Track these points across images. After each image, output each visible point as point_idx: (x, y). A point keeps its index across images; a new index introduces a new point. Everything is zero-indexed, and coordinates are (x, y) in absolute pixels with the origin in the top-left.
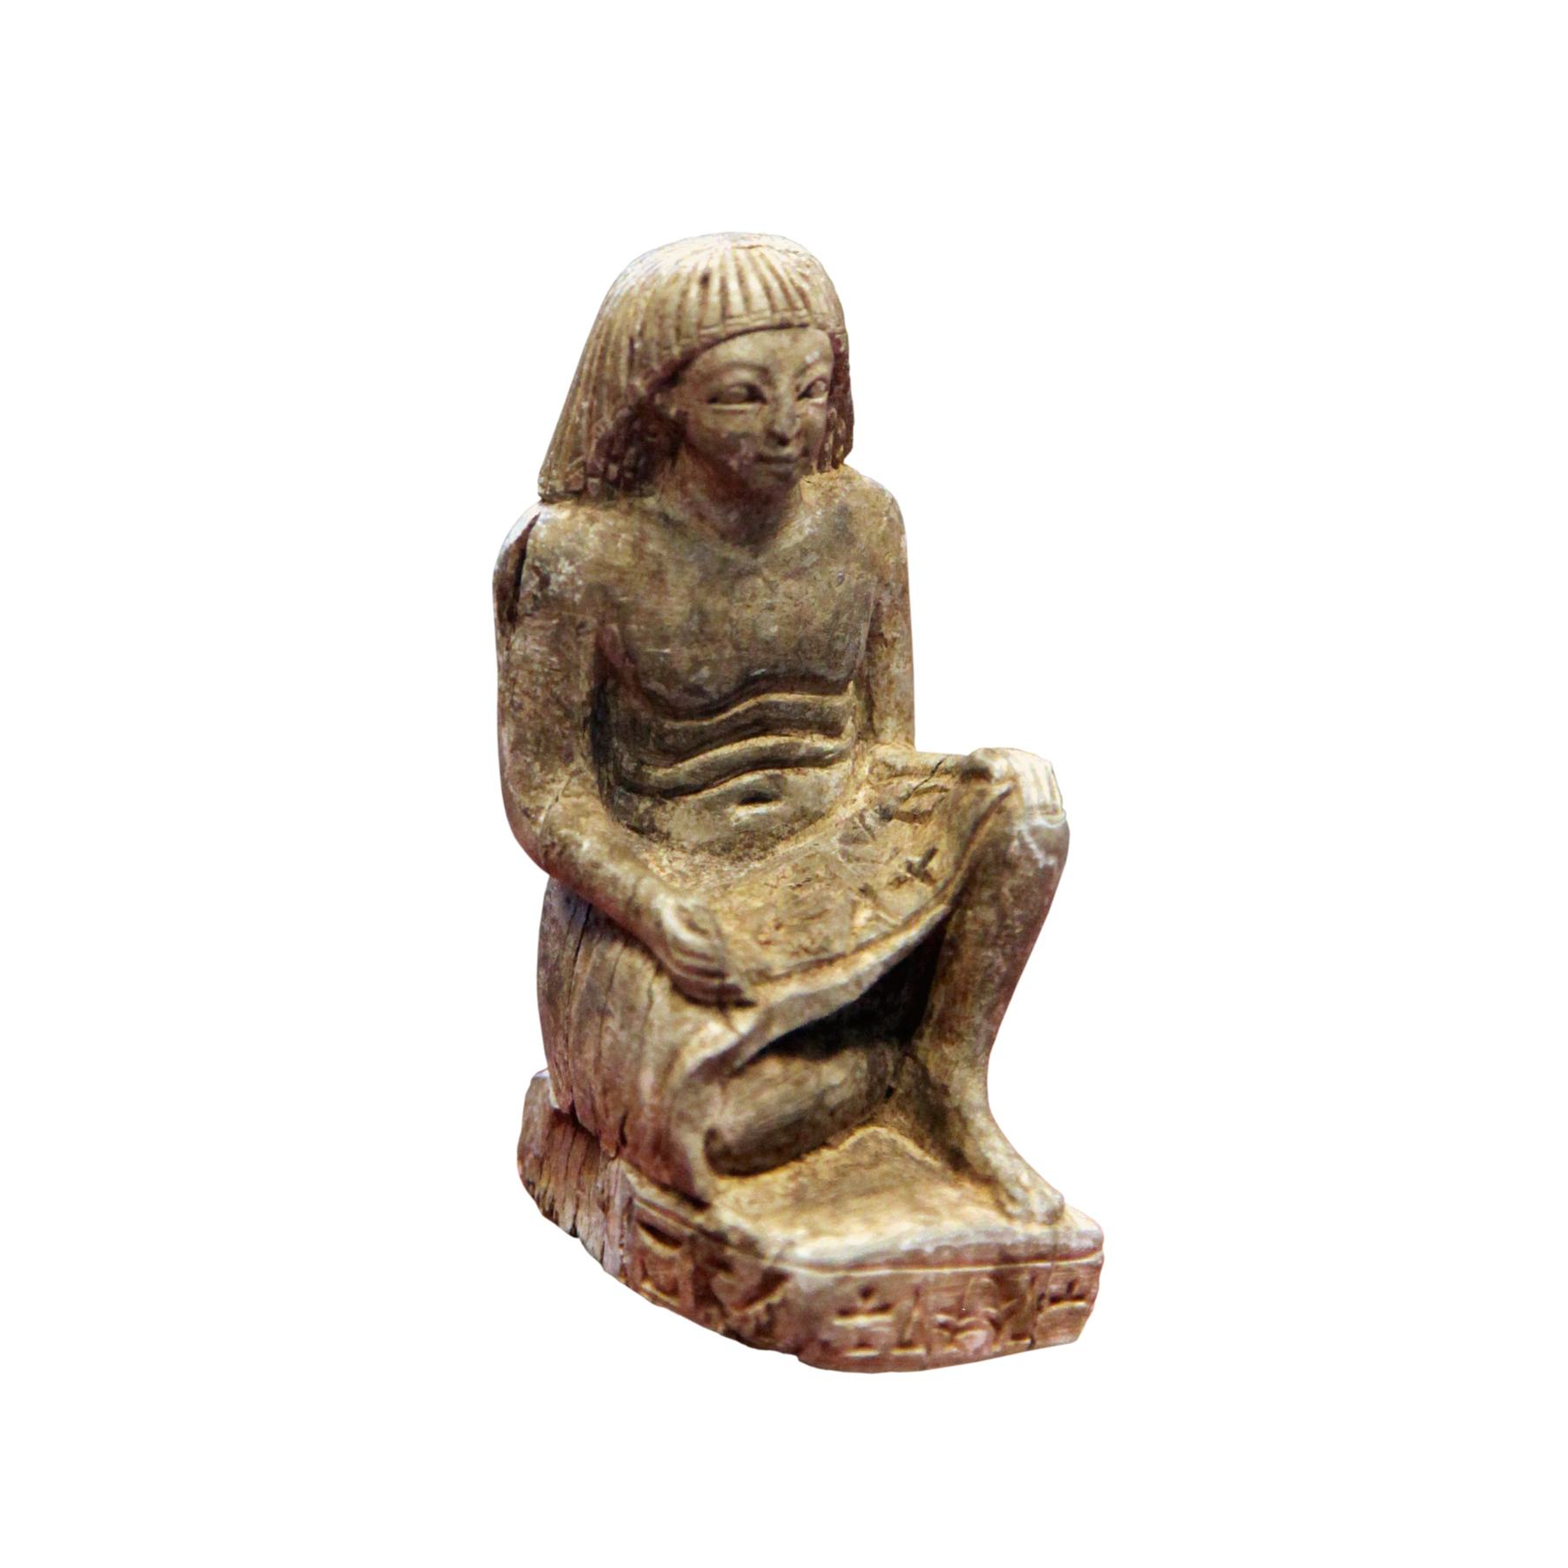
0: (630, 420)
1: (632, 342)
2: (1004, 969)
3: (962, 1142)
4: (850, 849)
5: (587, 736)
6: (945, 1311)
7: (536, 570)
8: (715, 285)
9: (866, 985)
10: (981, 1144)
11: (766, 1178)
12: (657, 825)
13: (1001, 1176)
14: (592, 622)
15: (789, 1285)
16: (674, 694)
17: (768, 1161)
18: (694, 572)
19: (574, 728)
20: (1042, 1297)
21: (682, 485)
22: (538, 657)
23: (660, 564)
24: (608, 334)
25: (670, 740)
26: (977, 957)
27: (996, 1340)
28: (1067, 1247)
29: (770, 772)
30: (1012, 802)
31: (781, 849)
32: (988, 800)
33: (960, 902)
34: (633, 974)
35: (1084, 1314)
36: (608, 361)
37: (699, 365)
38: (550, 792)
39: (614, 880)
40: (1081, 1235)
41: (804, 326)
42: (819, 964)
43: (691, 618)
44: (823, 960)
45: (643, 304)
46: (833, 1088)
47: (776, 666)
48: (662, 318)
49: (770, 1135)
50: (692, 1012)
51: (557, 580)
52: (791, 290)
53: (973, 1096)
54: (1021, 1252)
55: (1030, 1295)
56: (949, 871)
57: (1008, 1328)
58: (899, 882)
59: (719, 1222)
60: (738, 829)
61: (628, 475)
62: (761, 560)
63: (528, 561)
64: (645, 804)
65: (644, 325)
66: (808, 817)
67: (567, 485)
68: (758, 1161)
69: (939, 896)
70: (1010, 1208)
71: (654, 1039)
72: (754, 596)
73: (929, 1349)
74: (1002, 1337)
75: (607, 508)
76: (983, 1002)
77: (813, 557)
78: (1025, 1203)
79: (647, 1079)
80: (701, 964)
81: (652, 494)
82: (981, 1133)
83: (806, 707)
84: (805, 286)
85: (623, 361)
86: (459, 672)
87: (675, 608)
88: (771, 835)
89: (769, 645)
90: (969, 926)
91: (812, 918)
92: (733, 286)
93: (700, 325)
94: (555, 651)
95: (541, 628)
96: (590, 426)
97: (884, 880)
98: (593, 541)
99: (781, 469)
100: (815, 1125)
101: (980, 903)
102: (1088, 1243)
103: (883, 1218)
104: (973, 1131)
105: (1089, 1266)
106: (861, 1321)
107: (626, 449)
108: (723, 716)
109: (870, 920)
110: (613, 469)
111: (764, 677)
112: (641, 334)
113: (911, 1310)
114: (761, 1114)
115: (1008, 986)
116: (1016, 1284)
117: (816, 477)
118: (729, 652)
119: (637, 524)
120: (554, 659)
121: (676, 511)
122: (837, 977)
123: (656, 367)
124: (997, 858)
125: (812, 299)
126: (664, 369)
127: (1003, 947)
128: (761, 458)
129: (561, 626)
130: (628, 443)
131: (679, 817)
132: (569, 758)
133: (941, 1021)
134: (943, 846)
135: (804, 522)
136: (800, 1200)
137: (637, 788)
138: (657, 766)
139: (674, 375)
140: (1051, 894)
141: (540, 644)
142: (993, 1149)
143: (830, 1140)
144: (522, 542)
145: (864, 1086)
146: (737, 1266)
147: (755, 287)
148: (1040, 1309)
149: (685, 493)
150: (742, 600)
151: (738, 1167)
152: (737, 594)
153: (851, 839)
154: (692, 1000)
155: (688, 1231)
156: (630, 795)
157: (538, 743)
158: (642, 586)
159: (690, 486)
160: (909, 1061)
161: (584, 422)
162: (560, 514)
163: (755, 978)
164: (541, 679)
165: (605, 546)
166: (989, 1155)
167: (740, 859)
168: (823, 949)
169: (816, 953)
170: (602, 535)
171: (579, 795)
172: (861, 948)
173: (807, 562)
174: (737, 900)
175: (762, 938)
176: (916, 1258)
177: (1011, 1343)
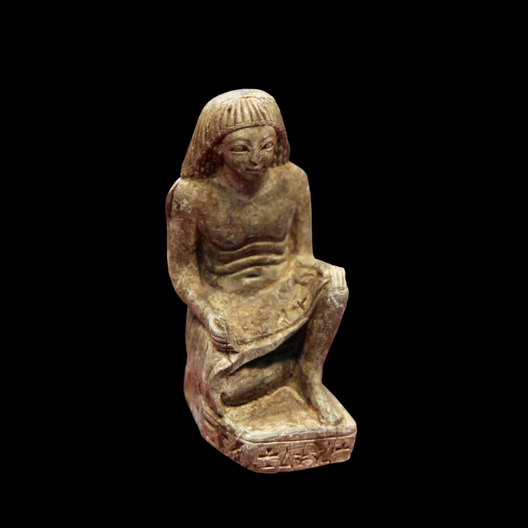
0: (206, 155)
1: (206, 130)
2: (326, 339)
3: (310, 395)
4: (281, 294)
5: (194, 255)
6: (297, 454)
7: (176, 202)
8: (233, 112)
9: (278, 345)
10: (316, 397)
11: (243, 407)
12: (218, 284)
13: (321, 409)
14: (194, 220)
15: (243, 446)
16: (222, 244)
17: (245, 401)
18: (228, 205)
19: (190, 253)
20: (333, 448)
21: (225, 175)
22: (177, 230)
23: (217, 202)
25: (222, 258)
27: (316, 463)
28: (341, 432)
29: (257, 267)
30: (329, 286)
31: (261, 292)
32: (321, 285)
33: (312, 317)
34: (204, 338)
36: (199, 135)
37: (227, 138)
38: (181, 274)
39: (198, 307)
40: (347, 429)
41: (263, 125)
42: (263, 337)
43: (227, 220)
44: (264, 336)
45: (210, 117)
46: (268, 377)
47: (257, 234)
48: (215, 122)
49: (244, 394)
50: (218, 354)
51: (183, 206)
52: (259, 112)
54: (325, 435)
56: (308, 307)
57: (321, 458)
58: (294, 308)
59: (225, 422)
60: (246, 286)
61: (208, 171)
62: (252, 199)
63: (174, 199)
64: (215, 277)
65: (210, 124)
66: (269, 282)
67: (188, 173)
68: (241, 402)
69: (305, 314)
70: (322, 421)
71: (206, 362)
72: (249, 212)
73: (292, 466)
74: (319, 461)
75: (200, 182)
76: (320, 349)
77: (271, 198)
78: (327, 419)
79: (204, 375)
80: (220, 339)
81: (215, 177)
82: (317, 393)
83: (269, 246)
84: (265, 111)
85: (203, 135)
87: (222, 216)
88: (256, 287)
89: (255, 228)
90: (315, 325)
91: (264, 320)
92: (239, 112)
93: (227, 126)
94: (182, 228)
95: (178, 221)
96: (194, 155)
97: (290, 307)
98: (195, 193)
99: (255, 173)
100: (261, 389)
101: (318, 318)
103: (278, 424)
104: (314, 392)
106: (268, 458)
107: (206, 163)
108: (240, 250)
109: (282, 321)
110: (203, 169)
111: (252, 238)
112: (209, 127)
113: (285, 454)
114: (240, 387)
116: (323, 445)
117: (276, 169)
118: (240, 230)
119: (210, 188)
120: (182, 231)
121: (223, 183)
122: (269, 342)
123: (213, 138)
124: (323, 304)
125: (267, 116)
126: (216, 139)
127: (326, 332)
128: (247, 169)
129: (184, 221)
130: (207, 161)
131: (226, 282)
132: (187, 263)
133: (307, 354)
134: (308, 298)
136: (253, 416)
137: (212, 271)
138: (219, 265)
139: (219, 141)
141: (177, 226)
142: (320, 399)
143: (268, 393)
145: (280, 375)
146: (229, 438)
147: (246, 111)
148: (332, 452)
149: (226, 177)
150: (245, 213)
151: (234, 404)
152: (243, 211)
153: (283, 291)
154: (219, 350)
155: (216, 424)
157: (177, 258)
158: (210, 209)
159: (228, 175)
160: (297, 366)
161: (192, 154)
163: (239, 343)
164: (178, 237)
165: (199, 195)
166: (318, 401)
167: (246, 296)
168: (265, 332)
169: (262, 333)
170: (198, 191)
171: (191, 275)
172: (278, 332)
173: (269, 199)
174: (241, 312)
175: (245, 328)
176: (286, 438)
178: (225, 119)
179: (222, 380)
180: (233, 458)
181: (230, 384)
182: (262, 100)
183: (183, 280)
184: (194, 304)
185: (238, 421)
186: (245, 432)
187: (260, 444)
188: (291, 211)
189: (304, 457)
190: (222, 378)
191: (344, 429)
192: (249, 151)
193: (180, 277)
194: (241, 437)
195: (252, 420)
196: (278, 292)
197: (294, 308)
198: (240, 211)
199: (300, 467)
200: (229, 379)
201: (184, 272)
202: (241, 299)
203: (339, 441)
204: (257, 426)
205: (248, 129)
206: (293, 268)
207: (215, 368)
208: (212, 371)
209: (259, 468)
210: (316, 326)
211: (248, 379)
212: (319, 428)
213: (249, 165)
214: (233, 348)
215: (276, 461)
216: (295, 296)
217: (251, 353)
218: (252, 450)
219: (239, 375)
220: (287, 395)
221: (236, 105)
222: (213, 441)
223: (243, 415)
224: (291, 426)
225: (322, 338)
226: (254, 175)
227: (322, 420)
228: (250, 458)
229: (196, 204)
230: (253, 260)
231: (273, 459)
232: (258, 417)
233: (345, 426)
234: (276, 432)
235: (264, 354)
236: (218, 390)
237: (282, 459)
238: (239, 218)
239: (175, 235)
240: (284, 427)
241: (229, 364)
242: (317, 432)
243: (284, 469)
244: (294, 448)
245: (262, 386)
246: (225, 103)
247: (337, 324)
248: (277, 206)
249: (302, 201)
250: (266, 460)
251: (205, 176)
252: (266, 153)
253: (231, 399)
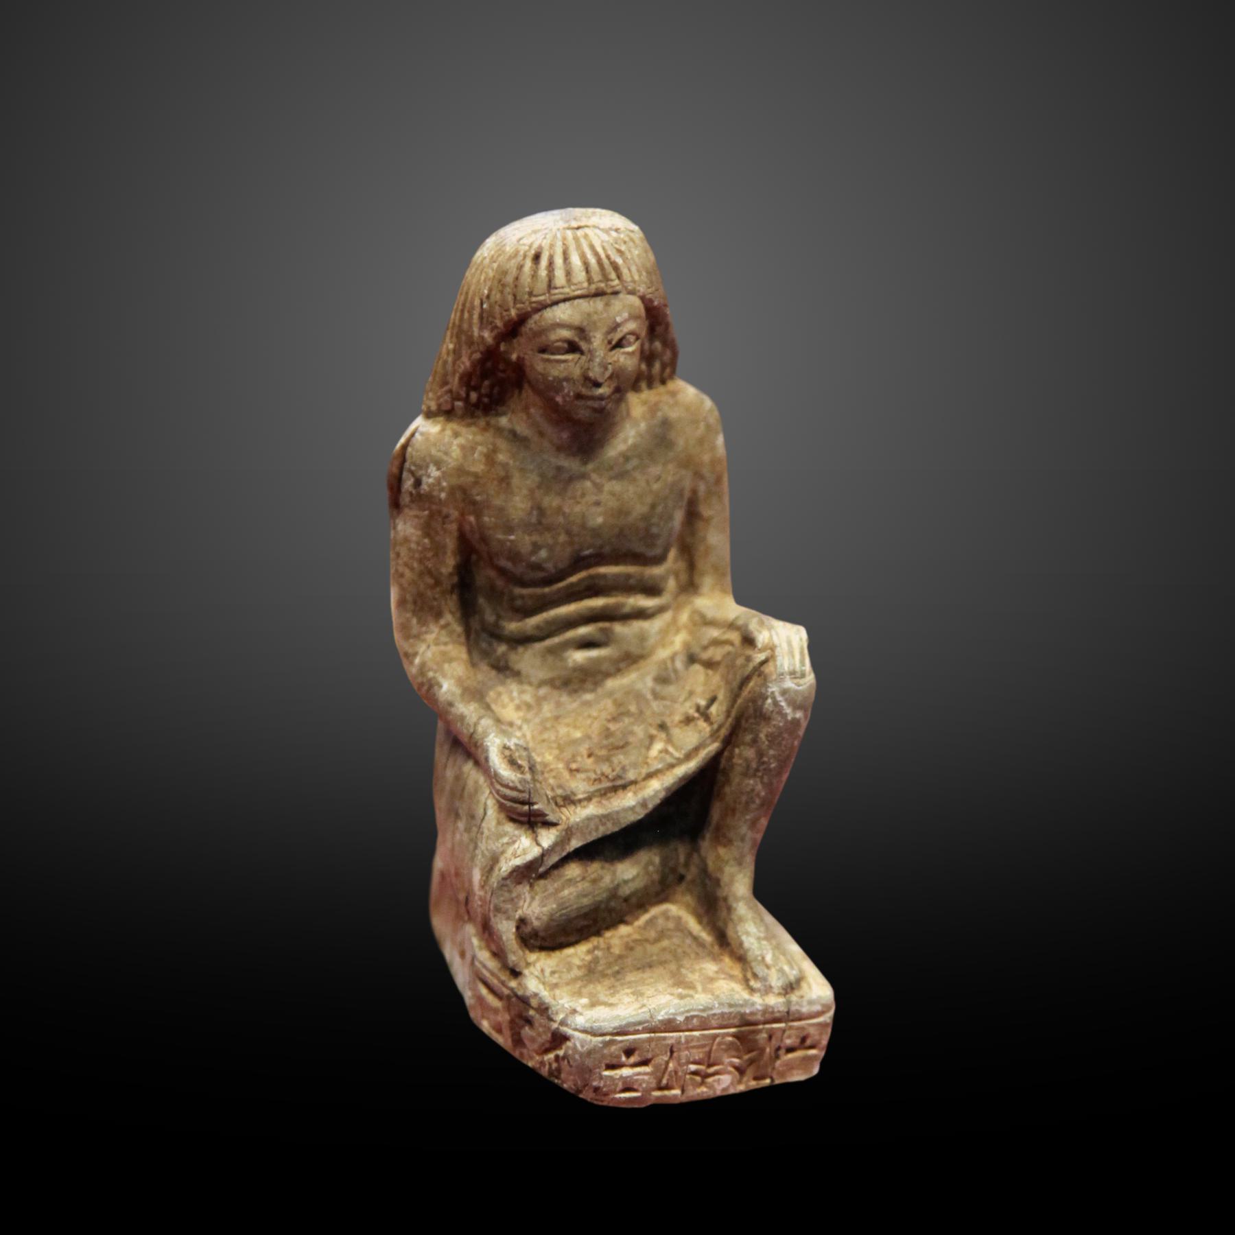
0: (482, 362)
1: (482, 304)
2: (763, 794)
3: (726, 924)
4: (658, 688)
5: (455, 597)
6: (695, 1063)
7: (412, 473)
8: (544, 262)
9: (651, 806)
10: (739, 928)
11: (569, 951)
12: (510, 664)
13: (750, 956)
14: (455, 514)
15: (569, 1044)
16: (519, 570)
17: (572, 939)
18: (533, 479)
19: (443, 593)
20: (779, 1049)
21: (526, 409)
22: (414, 538)
23: (507, 472)
25: (519, 603)
27: (740, 1082)
28: (798, 1011)
29: (601, 625)
30: (769, 669)
31: (610, 684)
32: (751, 666)
33: (730, 741)
34: (477, 790)
36: (466, 315)
37: (531, 324)
38: (424, 641)
39: (462, 718)
40: (811, 1002)
41: (616, 293)
42: (615, 789)
43: (530, 514)
44: (618, 786)
45: (491, 274)
46: (626, 882)
47: (601, 547)
48: (504, 286)
49: (570, 921)
50: (509, 828)
51: (427, 482)
52: (605, 261)
54: (759, 1017)
56: (721, 718)
57: (750, 1072)
58: (688, 720)
59: (526, 988)
60: (575, 669)
61: (486, 400)
62: (590, 466)
63: (407, 465)
64: (502, 649)
65: (490, 290)
66: (630, 659)
67: (439, 406)
68: (563, 939)
69: (714, 735)
70: (754, 984)
71: (482, 846)
72: (583, 495)
73: (683, 1091)
74: (745, 1079)
75: (469, 425)
76: (748, 817)
77: (635, 462)
78: (764, 979)
79: (477, 876)
80: (514, 794)
81: (504, 414)
82: (741, 919)
83: (629, 576)
84: (619, 261)
85: (476, 317)
87: (518, 505)
88: (600, 672)
89: (596, 532)
90: (736, 760)
91: (617, 748)
92: (559, 261)
93: (531, 294)
94: (427, 534)
95: (417, 517)
96: (454, 363)
97: (677, 718)
98: (456, 452)
99: (596, 404)
100: (610, 911)
101: (744, 744)
103: (649, 991)
104: (734, 917)
106: (626, 1072)
107: (483, 381)
108: (561, 585)
109: (661, 752)
110: (474, 396)
111: (590, 556)
112: (488, 297)
113: (667, 1063)
114: (562, 906)
116: (756, 1041)
117: (646, 394)
118: (562, 538)
119: (491, 439)
120: (426, 541)
121: (522, 429)
122: (628, 800)
123: (499, 323)
124: (755, 711)
125: (625, 271)
126: (505, 325)
127: (762, 778)
128: (579, 396)
129: (431, 516)
130: (484, 376)
131: (528, 660)
132: (438, 615)
133: (718, 828)
134: (721, 696)
136: (591, 972)
137: (496, 635)
138: (511, 620)
139: (513, 329)
141: (415, 528)
142: (748, 933)
143: (628, 918)
145: (656, 877)
146: (536, 1024)
147: (576, 260)
148: (777, 1057)
149: (528, 414)
150: (574, 498)
151: (546, 944)
152: (569, 494)
153: (663, 680)
154: (512, 820)
155: (506, 992)
157: (415, 603)
158: (492, 488)
159: (532, 410)
160: (695, 856)
161: (450, 359)
163: (560, 801)
164: (417, 555)
165: (465, 457)
166: (744, 938)
167: (576, 691)
168: (619, 777)
169: (614, 780)
170: (462, 447)
171: (446, 644)
172: (650, 776)
173: (629, 466)
174: (563, 730)
175: (574, 766)
176: (670, 1025)
178: (526, 278)
179: (520, 888)
180: (544, 1072)
181: (537, 898)
182: (614, 234)
183: (429, 654)
184: (453, 710)
185: (556, 986)
186: (574, 1011)
187: (608, 1038)
188: (681, 494)
189: (712, 1070)
190: (520, 883)
191: (805, 1003)
192: (582, 353)
193: (422, 648)
194: (563, 1023)
195: (590, 982)
196: (649, 682)
197: (688, 720)
198: (562, 493)
199: (702, 1092)
200: (536, 888)
201: (430, 637)
202: (565, 698)
203: (793, 1032)
204: (602, 997)
205: (581, 301)
206: (685, 627)
207: (502, 860)
208: (496, 869)
209: (606, 1094)
210: (740, 762)
211: (580, 886)
212: (746, 1001)
213: (583, 385)
214: (545, 815)
215: (646, 1078)
216: (691, 693)
217: (588, 826)
218: (589, 1053)
219: (560, 876)
220: (671, 925)
221: (552, 246)
222: (499, 1031)
223: (569, 970)
224: (681, 997)
225: (753, 790)
226: (595, 410)
227: (752, 983)
228: (585, 1071)
229: (459, 476)
230: (592, 609)
231: (639, 1074)
232: (604, 975)
233: (807, 997)
234: (644, 1009)
235: (616, 829)
236: (511, 913)
237: (659, 1074)
238: (559, 510)
239: (410, 549)
240: (663, 999)
241: (535, 852)
242: (742, 1010)
243: (665, 1096)
244: (687, 1048)
245: (613, 904)
246: (526, 241)
247: (788, 757)
248: (648, 482)
249: (705, 471)
250: (621, 1077)
251: (479, 413)
252: (622, 359)
253: (541, 934)
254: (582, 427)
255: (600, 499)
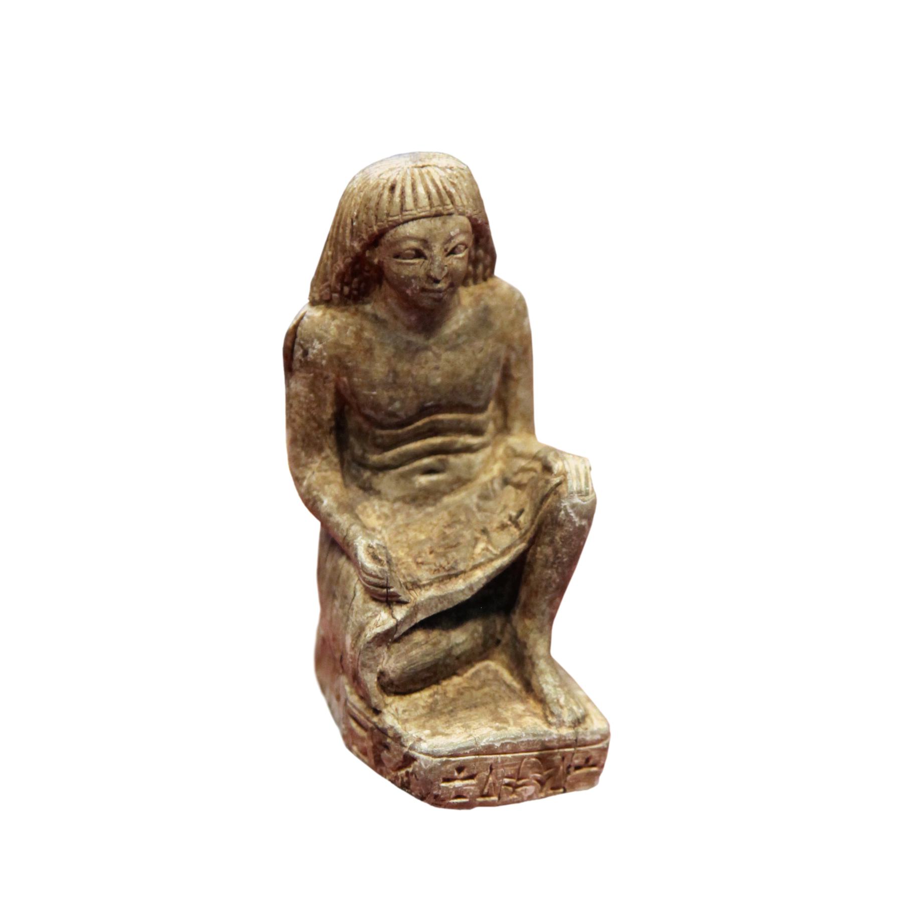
0: (353, 264)
1: (352, 222)
2: (558, 580)
3: (531, 676)
4: (481, 503)
5: (332, 436)
6: (508, 777)
7: (301, 346)
8: (398, 192)
9: (476, 589)
10: (540, 679)
11: (416, 695)
12: (373, 486)
13: (548, 699)
14: (332, 376)
15: (416, 763)
16: (379, 417)
18: (390, 350)
19: (324, 433)
20: (569, 767)
21: (385, 299)
22: (303, 394)
23: (371, 345)
24: (341, 214)
25: (379, 441)
26: (541, 573)
27: (541, 791)
28: (584, 739)
29: (439, 457)
30: (562, 489)
31: (446, 500)
32: (549, 487)
33: (533, 542)
34: (349, 577)
35: (598, 774)
36: (341, 231)
37: (388, 237)
38: (310, 468)
40: (593, 733)
41: (450, 214)
42: (449, 577)
43: (388, 376)
44: (452, 575)
45: (359, 200)
46: (458, 645)
47: (440, 400)
48: (368, 209)
49: (417, 673)
50: (372, 605)
51: (312, 353)
52: (443, 191)
53: (541, 650)
54: (555, 744)
55: (565, 765)
56: (527, 525)
57: (548, 784)
58: (503, 527)
59: (384, 722)
60: (420, 489)
61: (355, 292)
62: (432, 341)
63: (298, 340)
64: (367, 474)
65: (358, 212)
66: (461, 482)
67: (321, 297)
68: (411, 687)
69: (522, 537)
70: (551, 719)
71: (353, 618)
72: (426, 362)
73: (499, 798)
74: (545, 789)
75: (343, 311)
76: (547, 598)
77: (464, 338)
78: (559, 716)
79: (349, 641)
80: (376, 580)
81: (368, 303)
82: (542, 672)
83: (460, 421)
84: (453, 191)
85: (348, 231)
86: (264, 401)
87: (379, 369)
88: (438, 491)
89: (436, 389)
90: (538, 556)
91: (451, 547)
92: (409, 191)
93: (388, 215)
94: (312, 391)
95: (305, 378)
96: (332, 265)
97: (495, 525)
98: (333, 330)
99: (436, 296)
100: (446, 666)
101: (544, 544)
102: (598, 737)
103: (475, 725)
104: (537, 670)
105: (599, 749)
106: (458, 784)
107: (353, 279)
108: (410, 427)
109: (483, 550)
110: (346, 290)
111: (432, 407)
112: (357, 217)
113: (488, 777)
114: (411, 662)
115: (562, 588)
116: (553, 761)
117: (472, 288)
118: (411, 393)
119: (359, 321)
120: (312, 395)
121: (382, 313)
122: (459, 585)
123: (365, 236)
124: (552, 520)
125: (457, 198)
126: (369, 238)
127: (557, 569)
128: (423, 290)
129: (315, 377)
130: (354, 275)
131: (386, 482)
132: (320, 450)
133: (525, 606)
134: (527, 509)
135: (460, 317)
136: (432, 711)
137: (362, 464)
138: (374, 453)
139: (375, 241)
140: (584, 540)
141: (304, 386)
142: (547, 683)
143: (459, 671)
144: (295, 327)
145: (480, 641)
146: (392, 749)
147: (421, 190)
148: (568, 773)
149: (386, 303)
150: (420, 364)
151: (400, 690)
152: (416, 361)
153: (484, 497)
154: (374, 599)
155: (370, 725)
156: (359, 471)
157: (303, 441)
158: (360, 357)
159: (389, 300)
160: (508, 626)
161: (329, 263)
162: (317, 313)
163: (409, 586)
164: (305, 406)
165: (340, 334)
166: (544, 686)
167: (421, 505)
168: (452, 568)
169: (449, 570)
170: (338, 327)
171: (326, 471)
172: (475, 567)
173: (460, 341)
174: (412, 534)
175: (420, 560)
176: (490, 750)
177: (551, 792)
178: (385, 203)
179: (380, 649)
181: (393, 656)
182: (449, 171)
183: (314, 478)
184: (331, 519)
185: (406, 721)
186: (420, 740)
187: (444, 759)
188: (498, 361)
189: (520, 782)
190: (380, 646)
191: (588, 734)
192: (426, 258)
193: (308, 474)
194: (411, 748)
195: (431, 718)
196: (475, 499)
197: (503, 527)
198: (411, 360)
200: (392, 649)
201: (315, 466)
202: (413, 511)
203: (580, 754)
204: (440, 729)
205: (424, 220)
206: (501, 458)
207: (367, 629)
208: (363, 635)
210: (541, 557)
211: (424, 648)
212: (545, 732)
213: (426, 282)
214: (398, 596)
215: (472, 788)
216: (505, 507)
217: (430, 604)
218: (431, 770)
219: (410, 641)
220: (491, 676)
221: (403, 180)
223: (416, 709)
224: (498, 729)
225: (550, 578)
226: (435, 300)
227: (550, 719)
229: (336, 348)
230: (433, 445)
231: (467, 785)
232: (442, 713)
233: (590, 729)
234: (471, 738)
235: (451, 606)
236: (373, 667)
237: (482, 785)
238: (409, 373)
239: (300, 402)
240: (485, 730)
241: (391, 623)
242: (543, 739)
244: (503, 767)
245: (448, 661)
246: (385, 176)
248: (474, 352)
249: (516, 344)
250: (454, 787)
251: (350, 302)
252: (455, 262)
253: (396, 683)
254: (425, 312)
255: (438, 366)
